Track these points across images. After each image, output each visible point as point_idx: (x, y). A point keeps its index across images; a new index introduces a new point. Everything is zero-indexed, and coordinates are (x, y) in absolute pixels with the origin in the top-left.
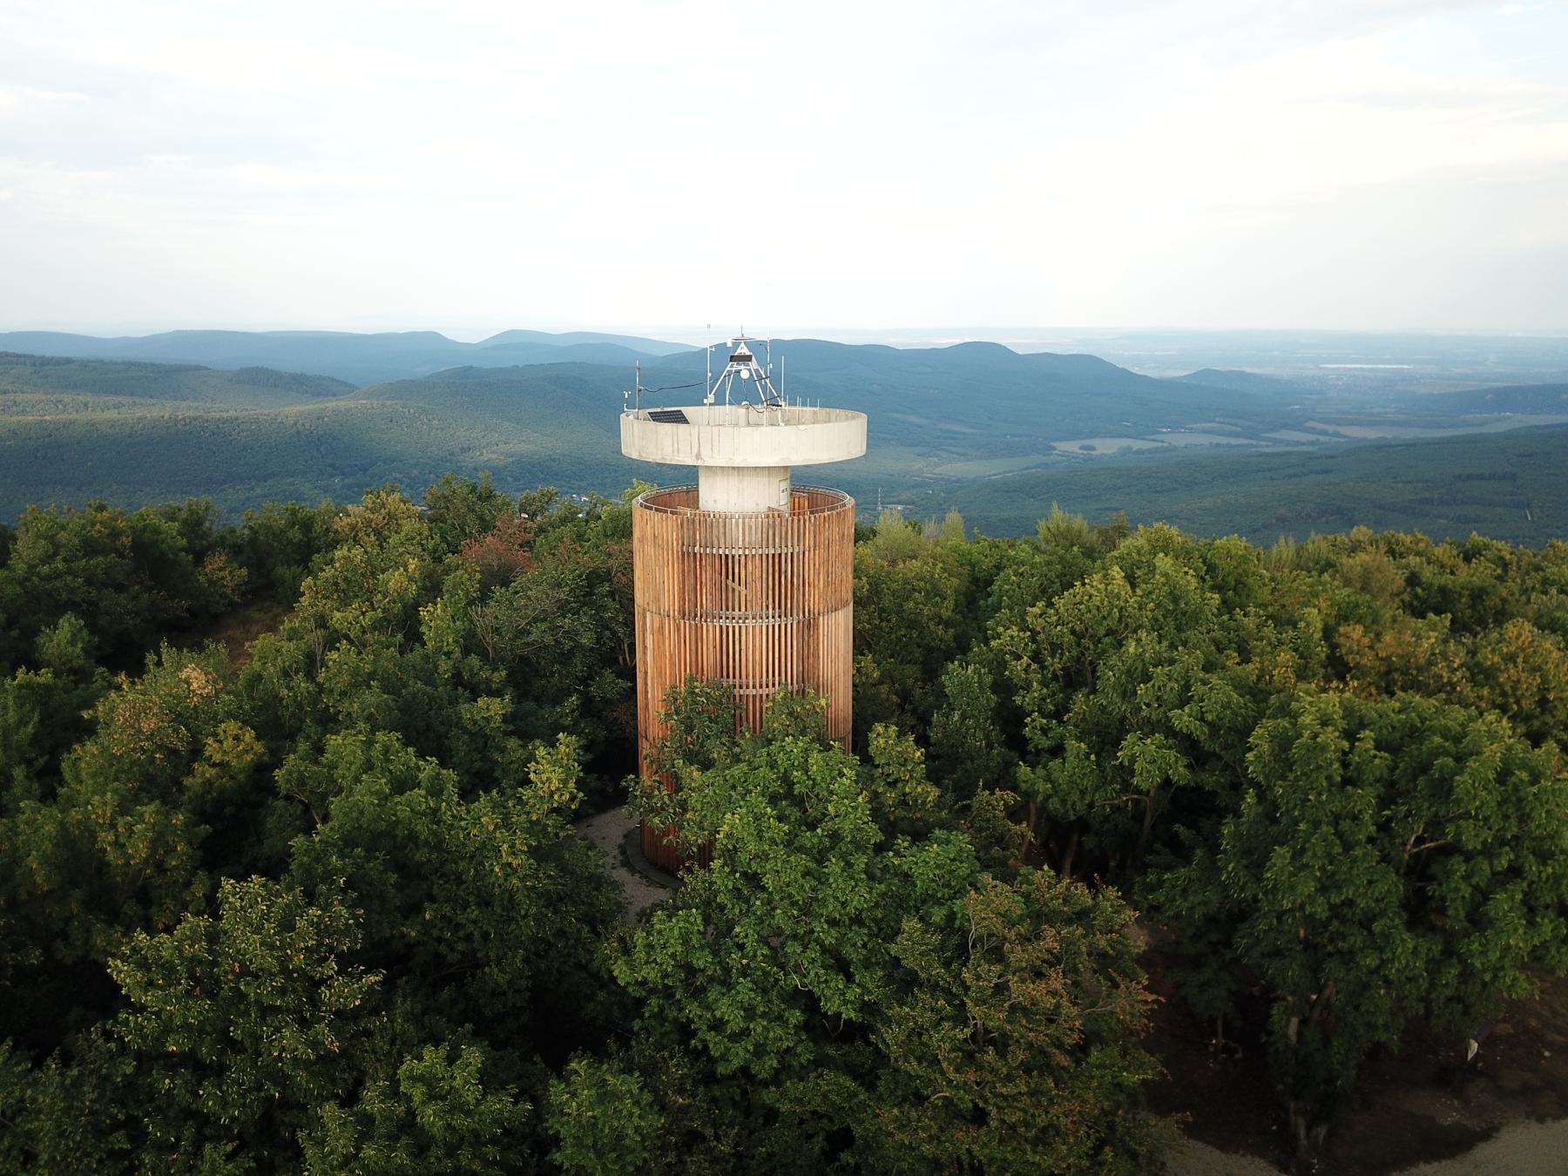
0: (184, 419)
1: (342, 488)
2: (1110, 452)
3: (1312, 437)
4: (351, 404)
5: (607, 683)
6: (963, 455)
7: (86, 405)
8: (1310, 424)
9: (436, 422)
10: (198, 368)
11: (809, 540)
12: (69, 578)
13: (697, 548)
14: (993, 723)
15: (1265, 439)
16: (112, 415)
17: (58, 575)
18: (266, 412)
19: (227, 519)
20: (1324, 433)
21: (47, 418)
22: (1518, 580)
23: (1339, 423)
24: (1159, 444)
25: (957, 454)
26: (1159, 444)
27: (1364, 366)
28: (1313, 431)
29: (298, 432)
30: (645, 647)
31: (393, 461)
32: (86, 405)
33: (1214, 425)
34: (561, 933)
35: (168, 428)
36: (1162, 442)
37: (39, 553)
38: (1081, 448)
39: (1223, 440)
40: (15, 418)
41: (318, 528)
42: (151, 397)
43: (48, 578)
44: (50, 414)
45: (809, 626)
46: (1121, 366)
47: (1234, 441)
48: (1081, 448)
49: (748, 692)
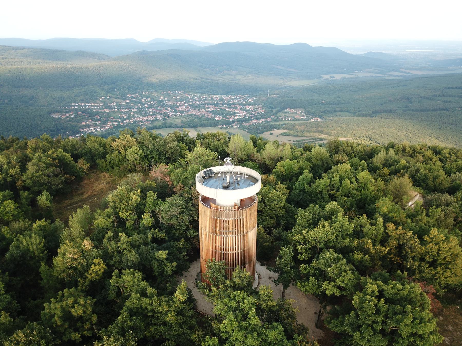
0: (60, 67)
1: (108, 89)
2: (339, 78)
3: (401, 74)
4: (109, 63)
5: (192, 233)
6: (295, 79)
7: (30, 62)
8: (401, 70)
9: (135, 68)
10: (63, 51)
11: (245, 215)
12: (43, 176)
13: (216, 218)
14: (292, 260)
15: (387, 75)
16: (38, 66)
17: (40, 176)
18: (84, 65)
19: (74, 98)
20: (405, 72)
21: (19, 67)
22: (449, 165)
23: (411, 69)
24: (354, 76)
25: (293, 78)
26: (354, 76)
27: (420, 51)
28: (402, 72)
29: (94, 72)
30: (202, 237)
31: (122, 81)
32: (30, 62)
33: (372, 70)
34: (183, 333)
35: (55, 70)
36: (355, 75)
37: (35, 170)
38: (330, 77)
39: (374, 75)
40: (10, 67)
41: (108, 146)
42: (49, 60)
43: (38, 177)
44: (20, 65)
45: (245, 236)
46: (344, 51)
47: (377, 75)
48: (330, 77)
49: (227, 252)
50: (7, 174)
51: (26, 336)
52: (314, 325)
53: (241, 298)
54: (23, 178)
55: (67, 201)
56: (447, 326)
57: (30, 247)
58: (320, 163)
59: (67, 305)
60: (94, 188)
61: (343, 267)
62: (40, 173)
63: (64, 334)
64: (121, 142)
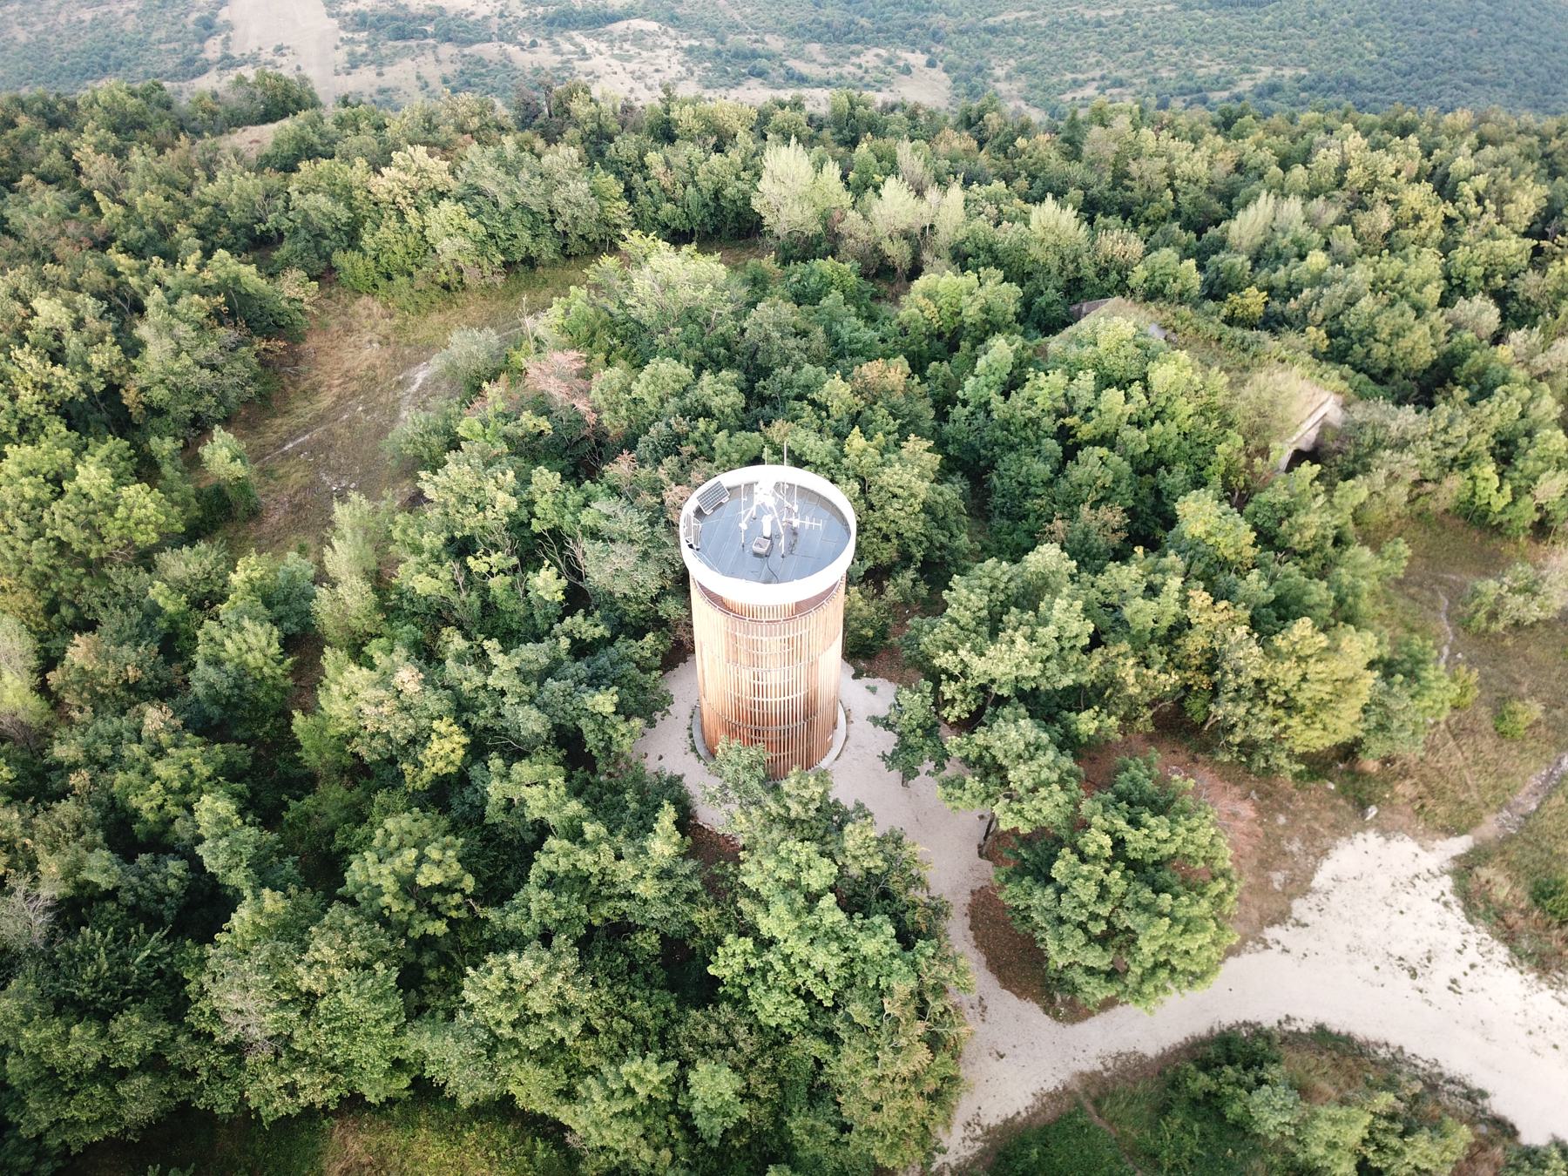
50: (88, 368)
51: (338, 951)
52: (976, 850)
53: (804, 859)
54: (141, 379)
55: (279, 421)
56: (1290, 840)
57: (249, 658)
58: (1054, 262)
59: (404, 865)
60: (347, 365)
61: (1045, 774)
62: (186, 360)
63: (409, 925)
64: (402, 175)
